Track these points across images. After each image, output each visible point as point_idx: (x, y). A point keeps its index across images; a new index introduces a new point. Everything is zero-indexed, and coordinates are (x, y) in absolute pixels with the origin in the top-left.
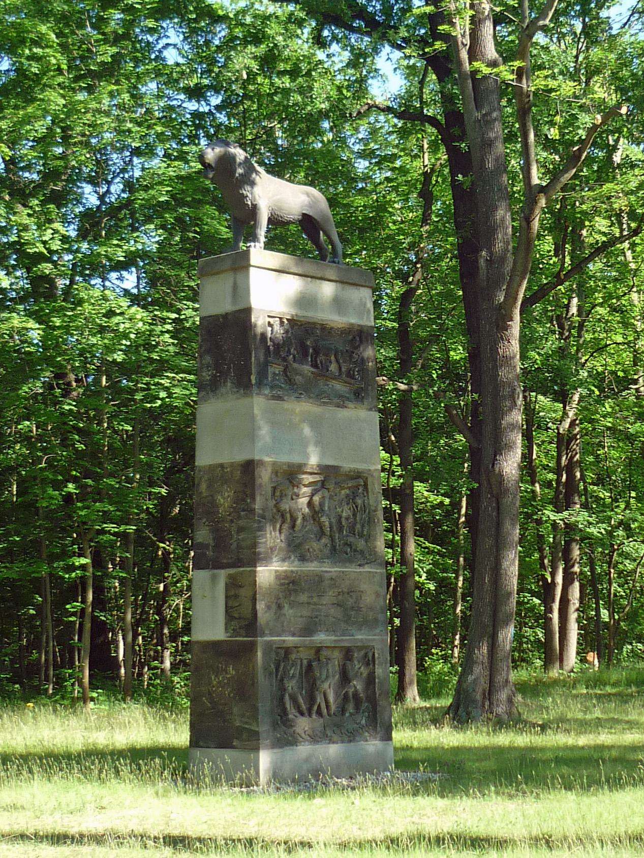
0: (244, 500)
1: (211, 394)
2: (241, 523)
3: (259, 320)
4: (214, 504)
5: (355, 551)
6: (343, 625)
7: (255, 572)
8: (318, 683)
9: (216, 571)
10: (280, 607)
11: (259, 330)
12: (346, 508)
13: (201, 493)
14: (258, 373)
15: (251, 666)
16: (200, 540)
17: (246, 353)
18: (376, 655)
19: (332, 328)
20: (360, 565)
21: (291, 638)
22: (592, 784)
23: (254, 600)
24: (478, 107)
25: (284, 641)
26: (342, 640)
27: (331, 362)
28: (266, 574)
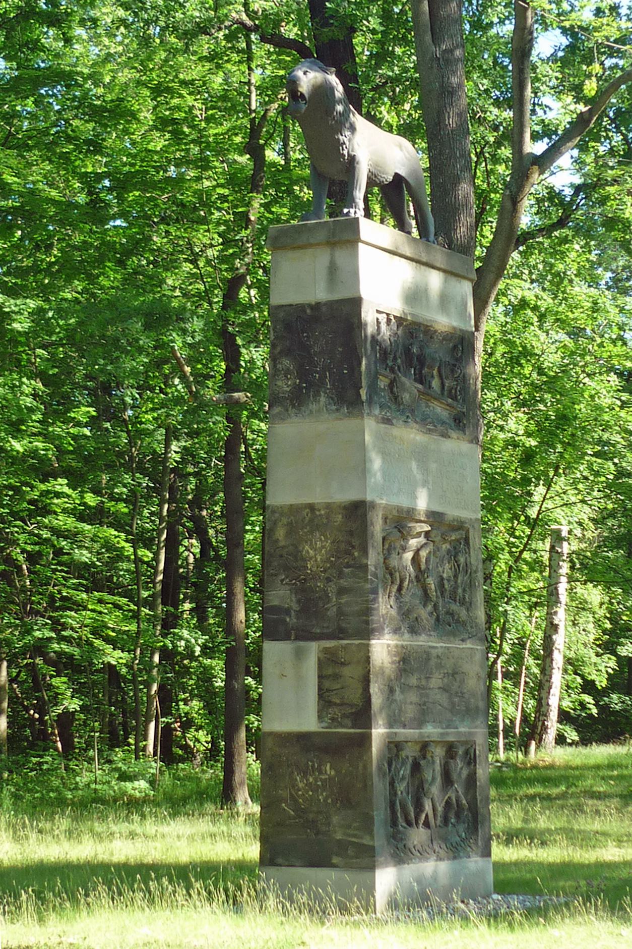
0: (348, 553)
1: (292, 411)
2: (343, 582)
3: (369, 315)
4: (297, 555)
5: (458, 621)
6: (449, 715)
7: (368, 645)
8: (426, 786)
9: (302, 643)
10: (391, 691)
11: (370, 330)
12: (447, 566)
13: (277, 541)
14: (369, 387)
15: (361, 765)
16: (276, 602)
17: (353, 357)
18: (477, 752)
19: (436, 331)
20: (463, 640)
21: (403, 730)
22: (538, 912)
23: (366, 681)
24: (436, 40)
25: (396, 733)
26: (447, 734)
27: (433, 377)
28: (383, 649)
